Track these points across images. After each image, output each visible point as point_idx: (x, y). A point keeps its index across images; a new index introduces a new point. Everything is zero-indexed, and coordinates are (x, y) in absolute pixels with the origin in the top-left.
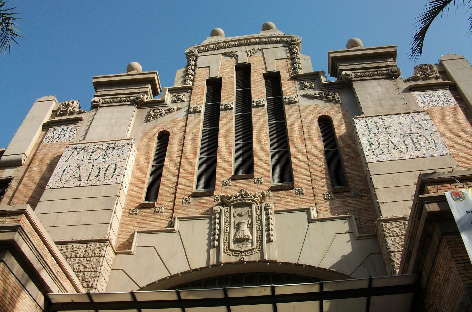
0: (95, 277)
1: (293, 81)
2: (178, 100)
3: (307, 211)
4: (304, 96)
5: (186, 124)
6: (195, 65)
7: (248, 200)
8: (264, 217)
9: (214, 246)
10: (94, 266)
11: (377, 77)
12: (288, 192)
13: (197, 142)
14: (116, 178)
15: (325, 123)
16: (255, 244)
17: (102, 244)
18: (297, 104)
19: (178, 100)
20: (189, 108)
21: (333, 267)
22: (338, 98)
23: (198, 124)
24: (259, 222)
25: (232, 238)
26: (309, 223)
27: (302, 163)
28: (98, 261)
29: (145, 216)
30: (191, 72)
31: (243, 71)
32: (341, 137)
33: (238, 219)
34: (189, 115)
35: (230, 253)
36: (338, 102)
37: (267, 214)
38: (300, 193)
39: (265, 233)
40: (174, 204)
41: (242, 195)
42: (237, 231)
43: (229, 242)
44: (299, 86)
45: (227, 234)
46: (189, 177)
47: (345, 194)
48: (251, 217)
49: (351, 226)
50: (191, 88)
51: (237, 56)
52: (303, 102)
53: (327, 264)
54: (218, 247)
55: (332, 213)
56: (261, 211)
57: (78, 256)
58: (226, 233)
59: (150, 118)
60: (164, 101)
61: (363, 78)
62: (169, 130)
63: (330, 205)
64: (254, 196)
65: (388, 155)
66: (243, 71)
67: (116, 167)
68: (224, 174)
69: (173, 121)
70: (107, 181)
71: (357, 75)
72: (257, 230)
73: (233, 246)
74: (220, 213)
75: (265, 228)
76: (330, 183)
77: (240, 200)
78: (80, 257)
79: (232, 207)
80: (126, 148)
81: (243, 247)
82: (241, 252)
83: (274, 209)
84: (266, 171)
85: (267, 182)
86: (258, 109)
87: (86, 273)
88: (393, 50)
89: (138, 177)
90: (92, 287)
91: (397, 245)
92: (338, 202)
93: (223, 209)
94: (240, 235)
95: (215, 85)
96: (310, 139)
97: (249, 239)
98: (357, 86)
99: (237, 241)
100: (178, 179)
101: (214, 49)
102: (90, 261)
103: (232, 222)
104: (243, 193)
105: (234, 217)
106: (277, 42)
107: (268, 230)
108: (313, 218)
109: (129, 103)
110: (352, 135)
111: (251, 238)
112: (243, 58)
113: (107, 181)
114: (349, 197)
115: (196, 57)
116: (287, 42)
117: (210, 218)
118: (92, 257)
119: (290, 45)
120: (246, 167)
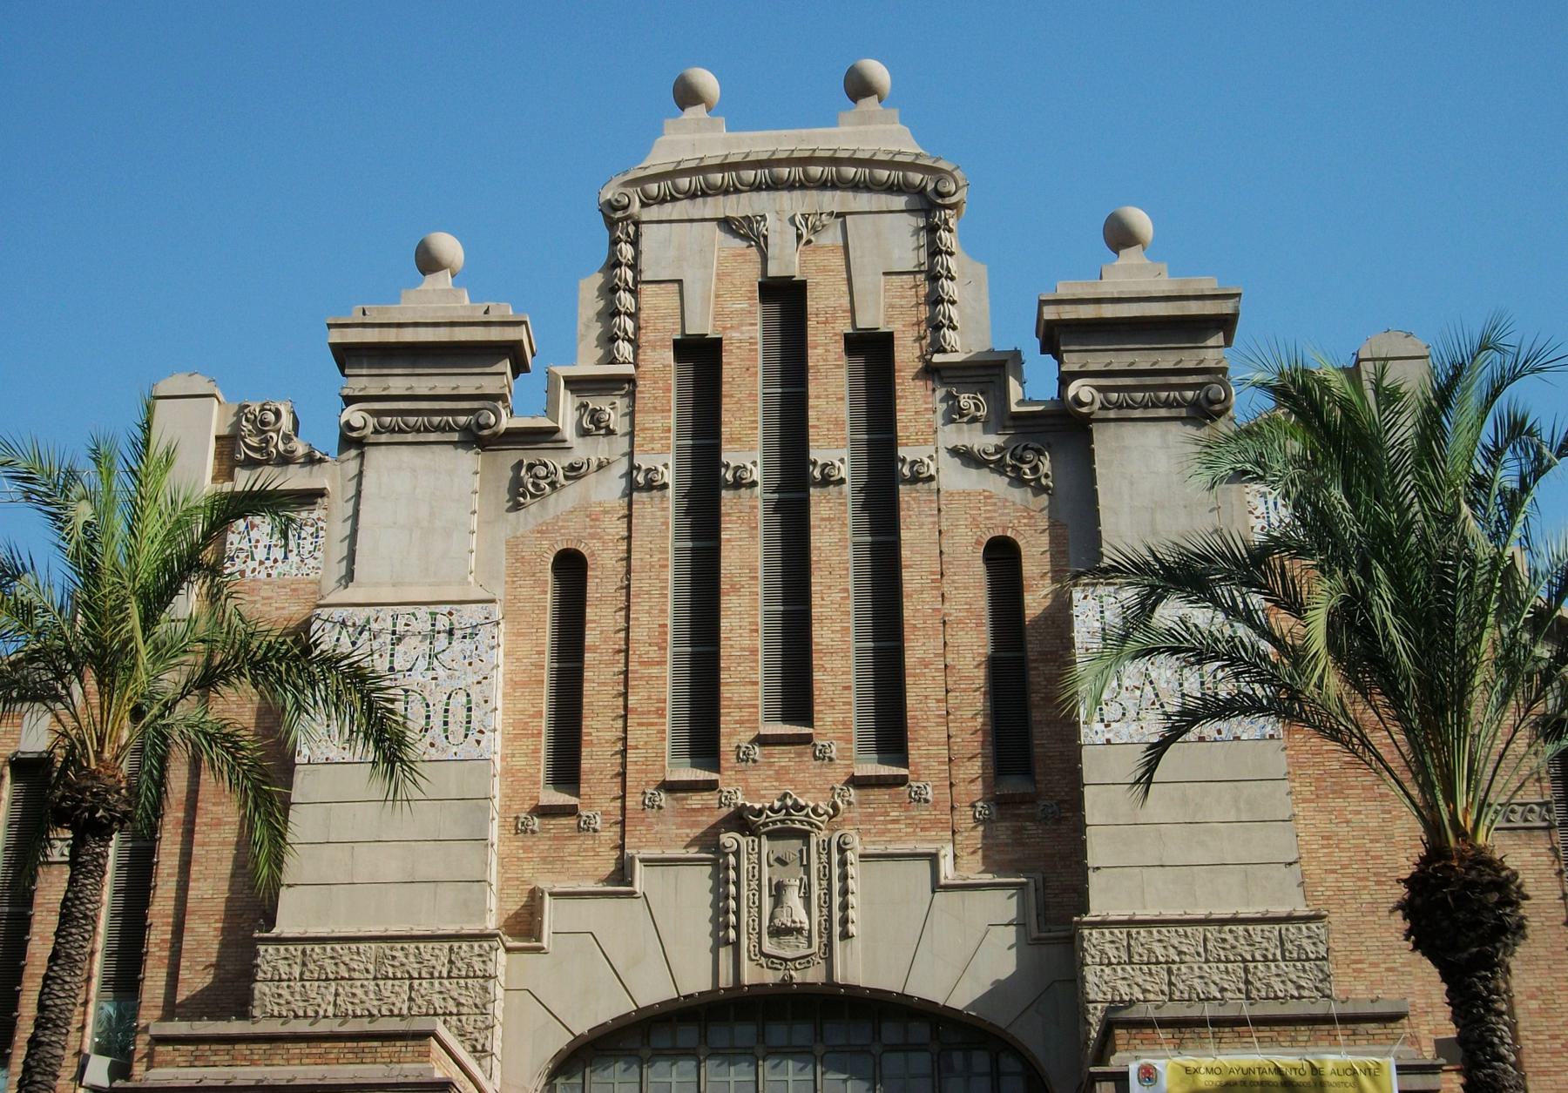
0: (487, 1028)
1: (930, 383)
2: (598, 428)
3: (933, 858)
4: (954, 452)
5: (630, 529)
6: (634, 266)
7: (801, 822)
8: (836, 871)
9: (727, 943)
10: (478, 1001)
11: (1163, 412)
12: (893, 791)
13: (665, 604)
14: (478, 742)
15: (1002, 557)
16: (816, 940)
17: (485, 945)
18: (934, 485)
19: (598, 428)
20: (633, 467)
21: (973, 1005)
22: (1046, 476)
23: (661, 519)
24: (824, 883)
25: (766, 922)
26: (933, 892)
27: (932, 704)
28: (485, 990)
29: (555, 838)
30: (626, 299)
31: (785, 299)
32: (1037, 620)
33: (779, 874)
34: (635, 495)
35: (763, 961)
36: (1045, 489)
37: (843, 863)
38: (920, 800)
39: (837, 915)
40: (624, 808)
41: (787, 808)
42: (775, 906)
43: (760, 933)
44: (944, 406)
45: (754, 911)
46: (652, 724)
47: (1023, 810)
48: (807, 869)
49: (1022, 907)
50: (631, 380)
51: (765, 237)
52: (954, 478)
53: (960, 1000)
54: (736, 945)
55: (990, 865)
56: (829, 854)
57: (436, 974)
58: (753, 909)
59: (524, 496)
60: (556, 430)
61: (1123, 411)
62: (582, 548)
63: (984, 837)
64: (814, 810)
65: (1134, 726)
66: (785, 299)
67: (469, 702)
68: (741, 722)
69: (587, 508)
70: (455, 749)
71: (1109, 402)
72: (820, 906)
73: (768, 946)
74: (737, 854)
75: (837, 900)
76: (989, 750)
77: (782, 821)
78: (440, 977)
79: (764, 838)
80: (484, 633)
81: (791, 948)
82: (786, 960)
83: (860, 850)
84: (843, 723)
85: (844, 758)
86: (824, 491)
87: (464, 1018)
88: (1225, 308)
89: (522, 712)
90: (484, 1051)
91: (1104, 988)
92: (1003, 831)
93: (743, 841)
94: (783, 919)
95: (700, 356)
96: (959, 622)
97: (802, 928)
98: (1105, 441)
99: (778, 932)
100: (625, 730)
101: (692, 195)
102: (467, 988)
103: (765, 882)
104: (789, 802)
105: (770, 865)
106: (891, 188)
107: (845, 907)
108: (943, 881)
109: (455, 437)
110: (1060, 617)
111: (806, 926)
112: (786, 261)
113: (455, 749)
114: (1032, 818)
115: (637, 224)
116: (920, 191)
117: (714, 863)
118: (467, 977)
119: (928, 204)
120: (795, 695)
